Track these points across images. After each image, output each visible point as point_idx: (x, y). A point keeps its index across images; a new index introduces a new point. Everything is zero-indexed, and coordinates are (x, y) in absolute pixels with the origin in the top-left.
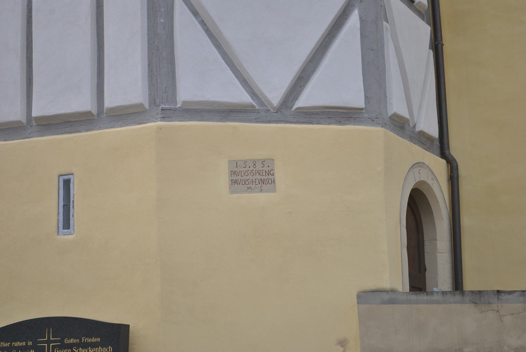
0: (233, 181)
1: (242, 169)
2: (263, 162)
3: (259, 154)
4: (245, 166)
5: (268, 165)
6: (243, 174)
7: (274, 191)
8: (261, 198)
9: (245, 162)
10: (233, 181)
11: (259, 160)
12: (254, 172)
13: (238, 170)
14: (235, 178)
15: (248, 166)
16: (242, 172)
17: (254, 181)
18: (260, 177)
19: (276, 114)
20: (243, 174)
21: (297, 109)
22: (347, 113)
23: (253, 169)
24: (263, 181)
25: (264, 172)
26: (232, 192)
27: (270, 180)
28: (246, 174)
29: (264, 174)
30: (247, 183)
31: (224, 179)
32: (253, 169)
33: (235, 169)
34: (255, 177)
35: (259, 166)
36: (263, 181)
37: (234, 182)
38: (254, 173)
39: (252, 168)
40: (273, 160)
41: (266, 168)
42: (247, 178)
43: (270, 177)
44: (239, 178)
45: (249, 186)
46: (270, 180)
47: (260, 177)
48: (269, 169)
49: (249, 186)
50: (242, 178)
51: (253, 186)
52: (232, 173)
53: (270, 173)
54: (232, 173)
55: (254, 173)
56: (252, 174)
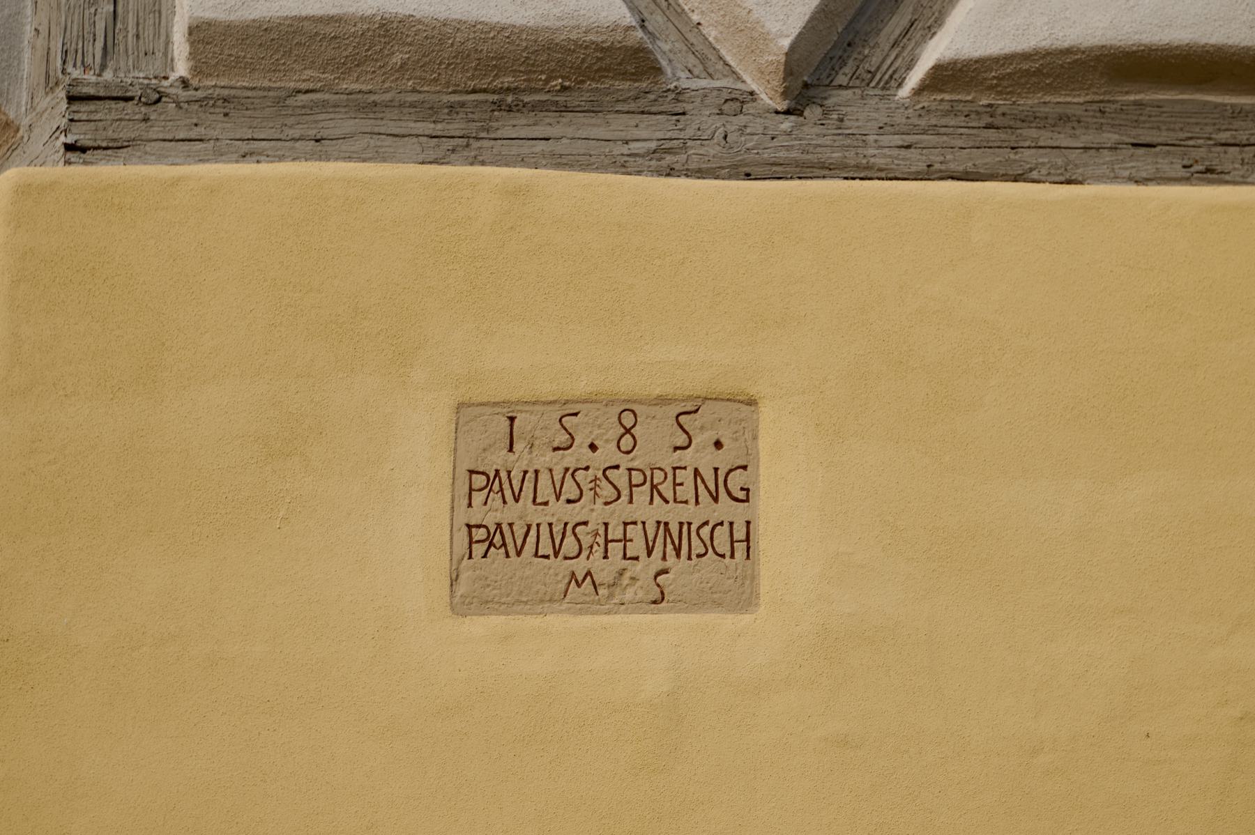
0: (480, 534)
1: (545, 459)
2: (686, 412)
3: (669, 359)
4: (562, 438)
5: (711, 436)
6: (545, 491)
7: (743, 597)
8: (633, 648)
9: (569, 411)
10: (480, 534)
11: (662, 401)
12: (619, 477)
13: (520, 461)
14: (491, 513)
15: (582, 440)
16: (544, 479)
17: (616, 532)
18: (659, 511)
19: (787, 123)
20: (545, 491)
21: (946, 76)
22: (1191, 138)
23: (618, 458)
24: (673, 538)
25: (686, 476)
26: (461, 606)
27: (722, 534)
28: (570, 490)
29: (686, 492)
30: (570, 545)
31: (420, 514)
32: (618, 458)
33: (497, 459)
34: (622, 510)
35: (656, 441)
36: (673, 538)
37: (489, 539)
38: (623, 484)
39: (606, 454)
40: (751, 403)
41: (701, 457)
42: (574, 513)
43: (725, 509)
44: (510, 513)
45: (580, 566)
46: (722, 534)
47: (659, 511)
48: (723, 460)
49: (580, 566)
50: (536, 516)
51: (604, 570)
52: (479, 481)
53: (730, 485)
54: (479, 481)
55: (623, 484)
56: (607, 491)
